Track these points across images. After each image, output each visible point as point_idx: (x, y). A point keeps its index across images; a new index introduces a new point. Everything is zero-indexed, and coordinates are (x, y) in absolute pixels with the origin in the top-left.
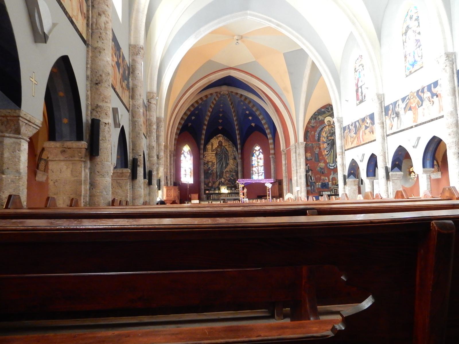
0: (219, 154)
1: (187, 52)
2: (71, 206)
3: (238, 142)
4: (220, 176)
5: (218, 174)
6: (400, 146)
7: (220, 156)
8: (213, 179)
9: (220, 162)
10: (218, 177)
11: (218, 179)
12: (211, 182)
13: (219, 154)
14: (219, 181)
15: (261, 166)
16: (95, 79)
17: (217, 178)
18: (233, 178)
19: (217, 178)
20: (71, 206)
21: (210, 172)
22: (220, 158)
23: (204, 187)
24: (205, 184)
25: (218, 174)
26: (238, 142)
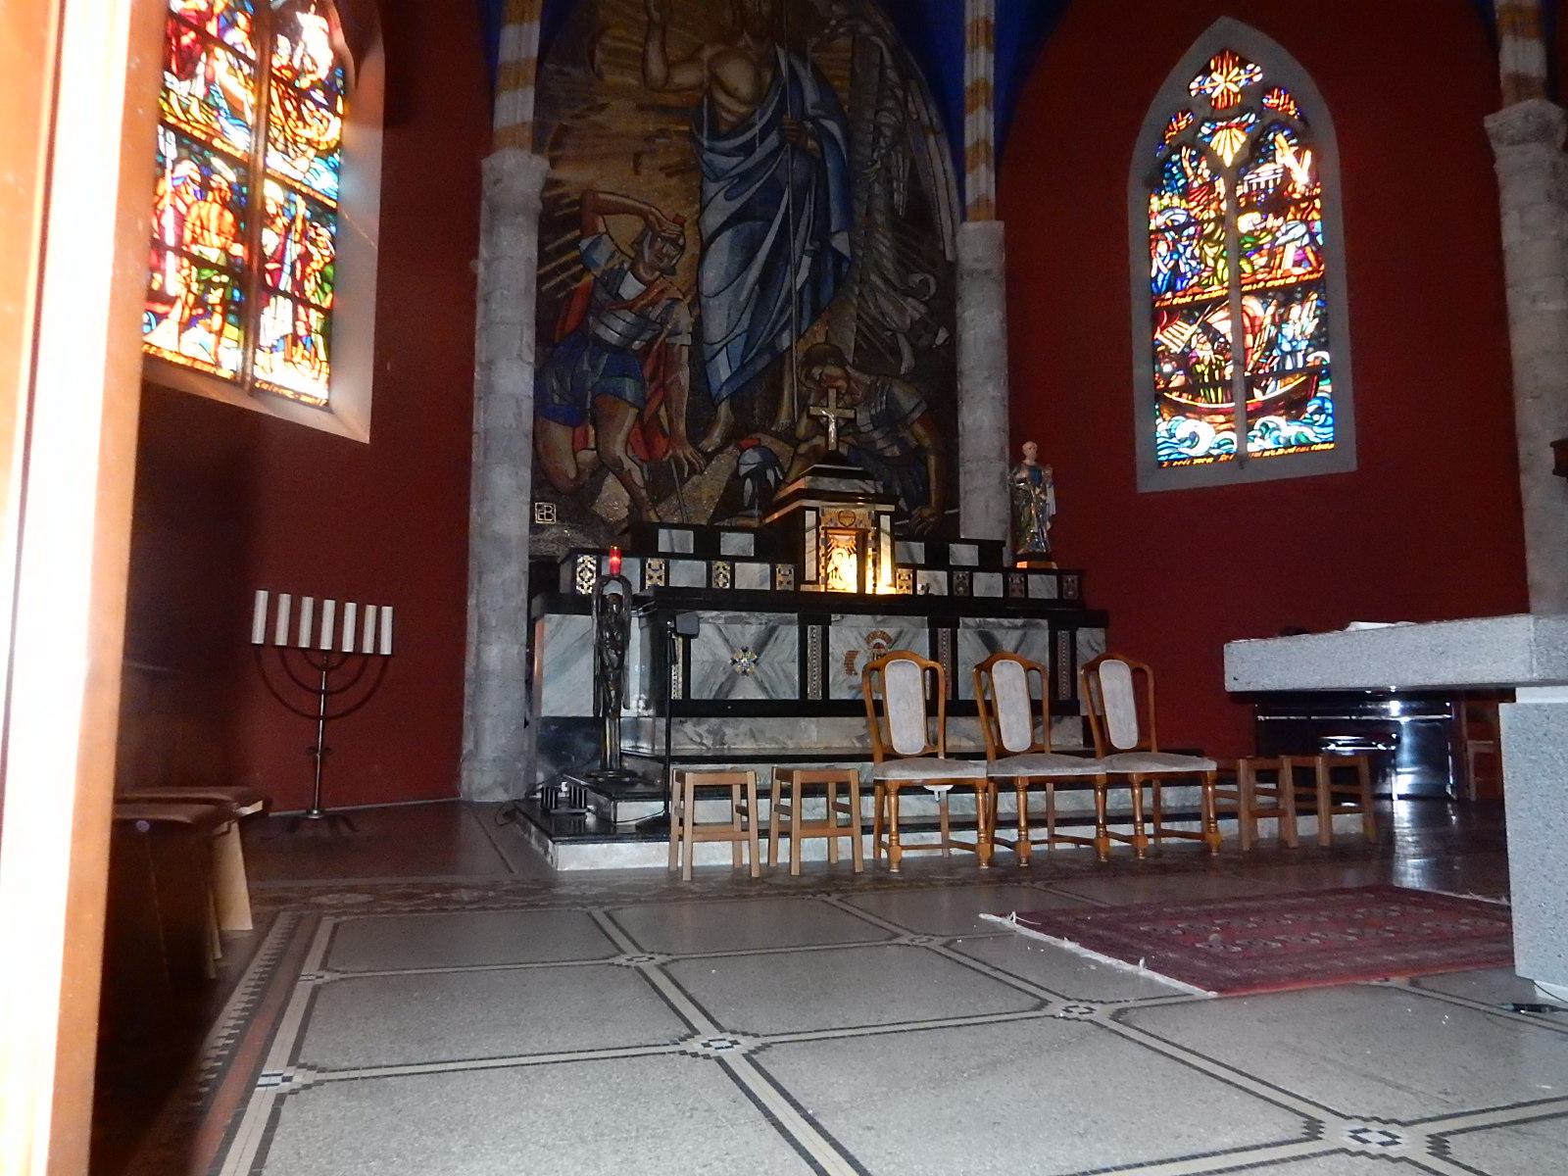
0: (737, 129)
1: (379, 182)
2: (694, 824)
3: (979, 66)
4: (737, 401)
5: (722, 370)
6: (1554, 473)
7: (748, 149)
8: (647, 431)
9: (746, 227)
10: (724, 410)
11: (716, 436)
12: (628, 464)
13: (737, 129)
14: (723, 464)
15: (1287, 296)
16: (963, 1120)
17: (699, 426)
18: (901, 442)
19: (699, 426)
20: (694, 824)
21: (612, 337)
22: (745, 177)
23: (535, 528)
24: (543, 484)
25: (722, 370)
26: (979, 66)
